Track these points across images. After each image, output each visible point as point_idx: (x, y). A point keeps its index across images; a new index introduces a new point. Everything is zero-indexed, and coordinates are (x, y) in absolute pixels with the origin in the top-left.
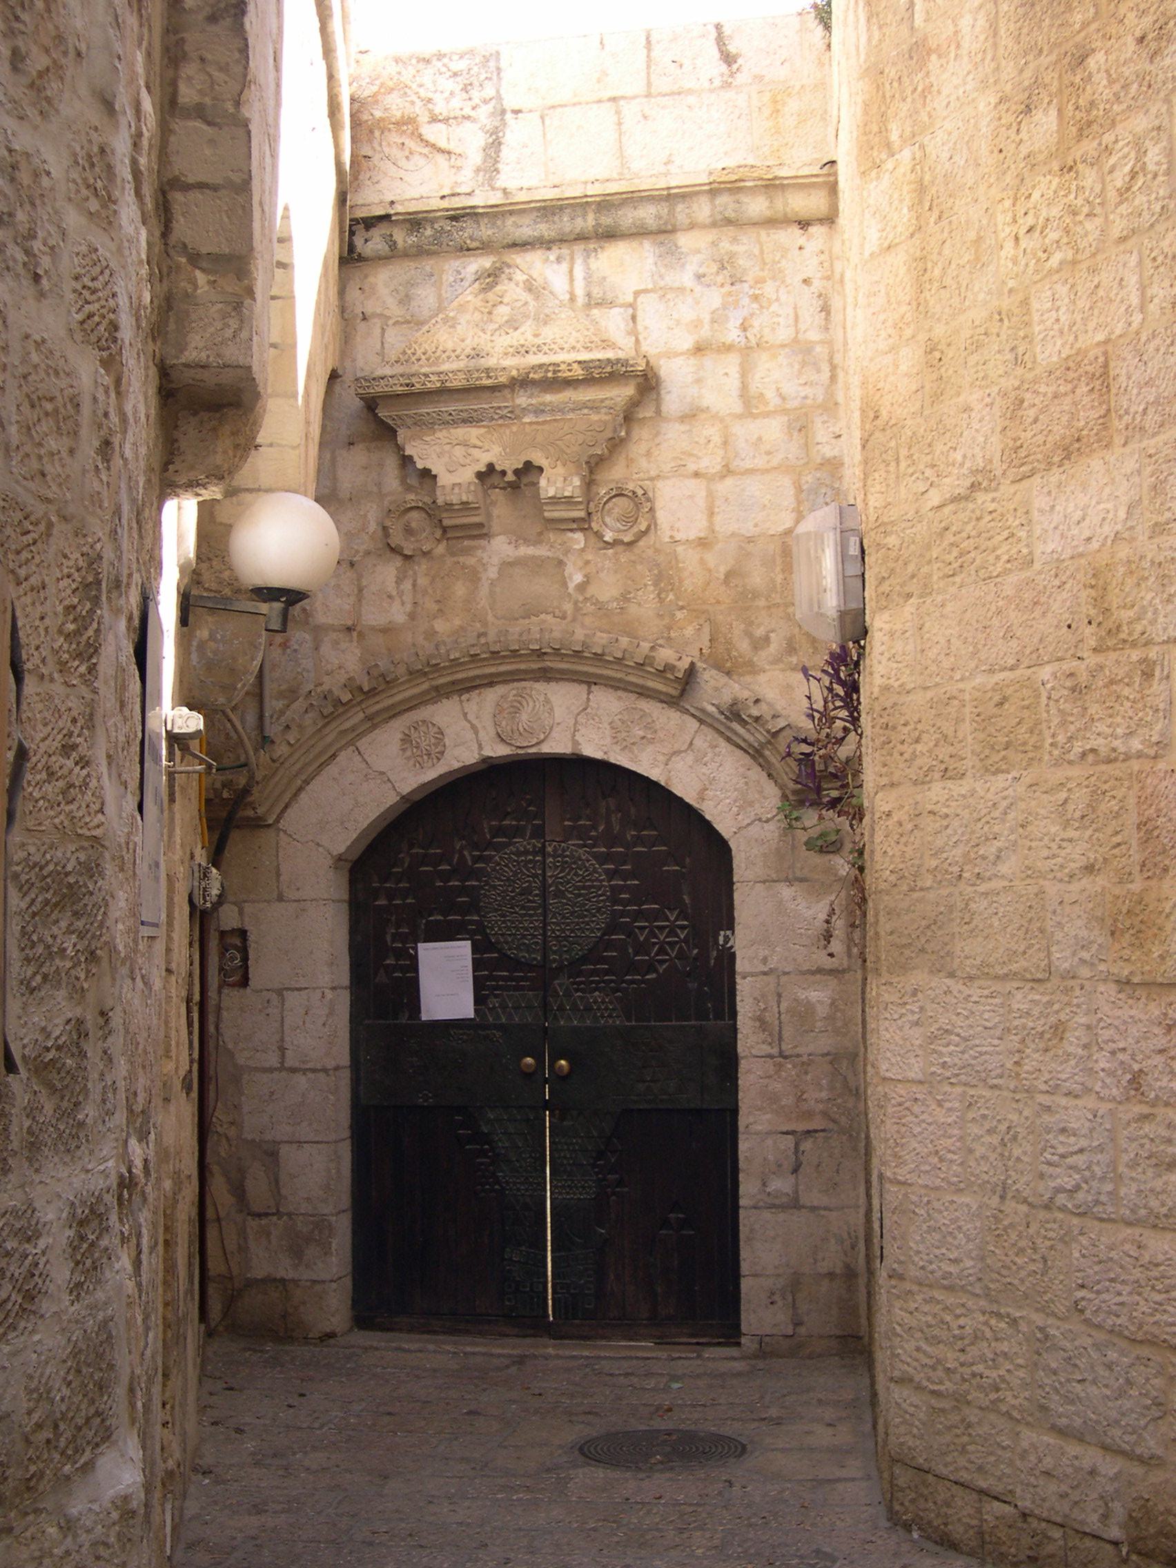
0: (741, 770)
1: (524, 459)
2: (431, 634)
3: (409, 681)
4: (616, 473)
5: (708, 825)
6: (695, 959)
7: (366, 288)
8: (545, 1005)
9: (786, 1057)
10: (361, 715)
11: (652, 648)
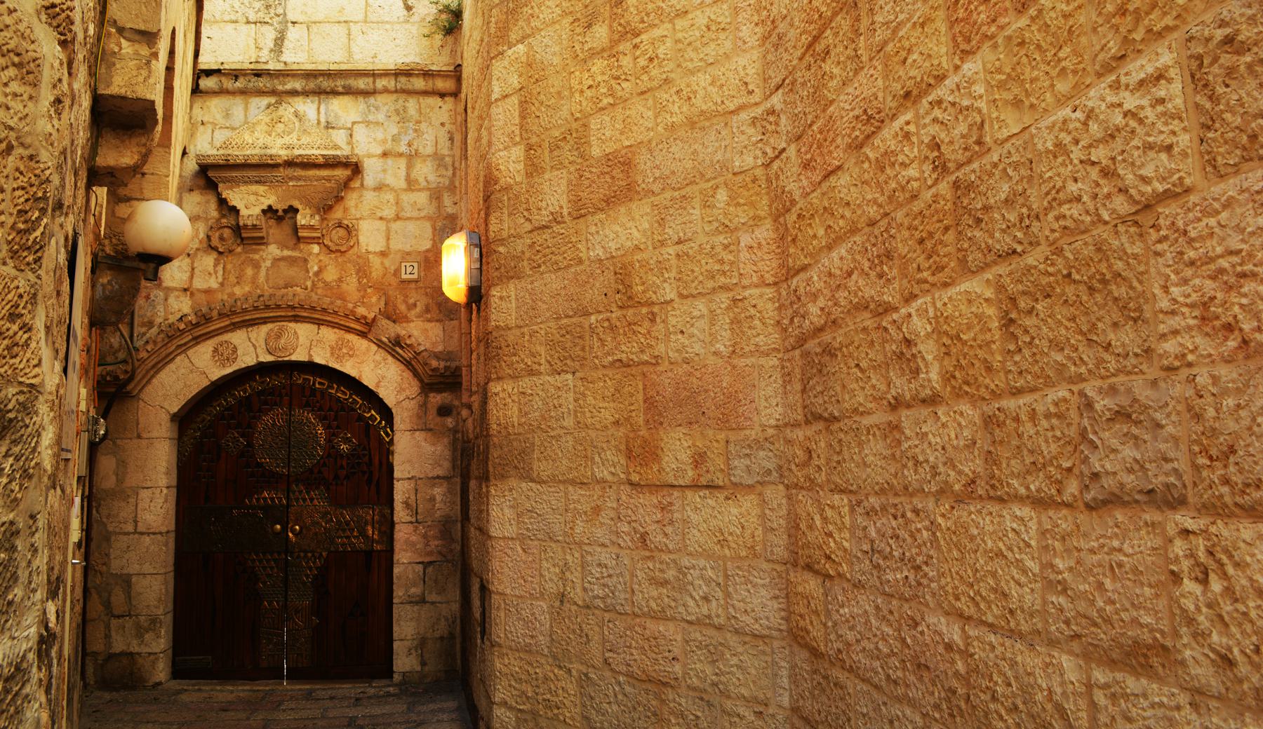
1: (288, 204)
4: (337, 214)
5: (381, 400)
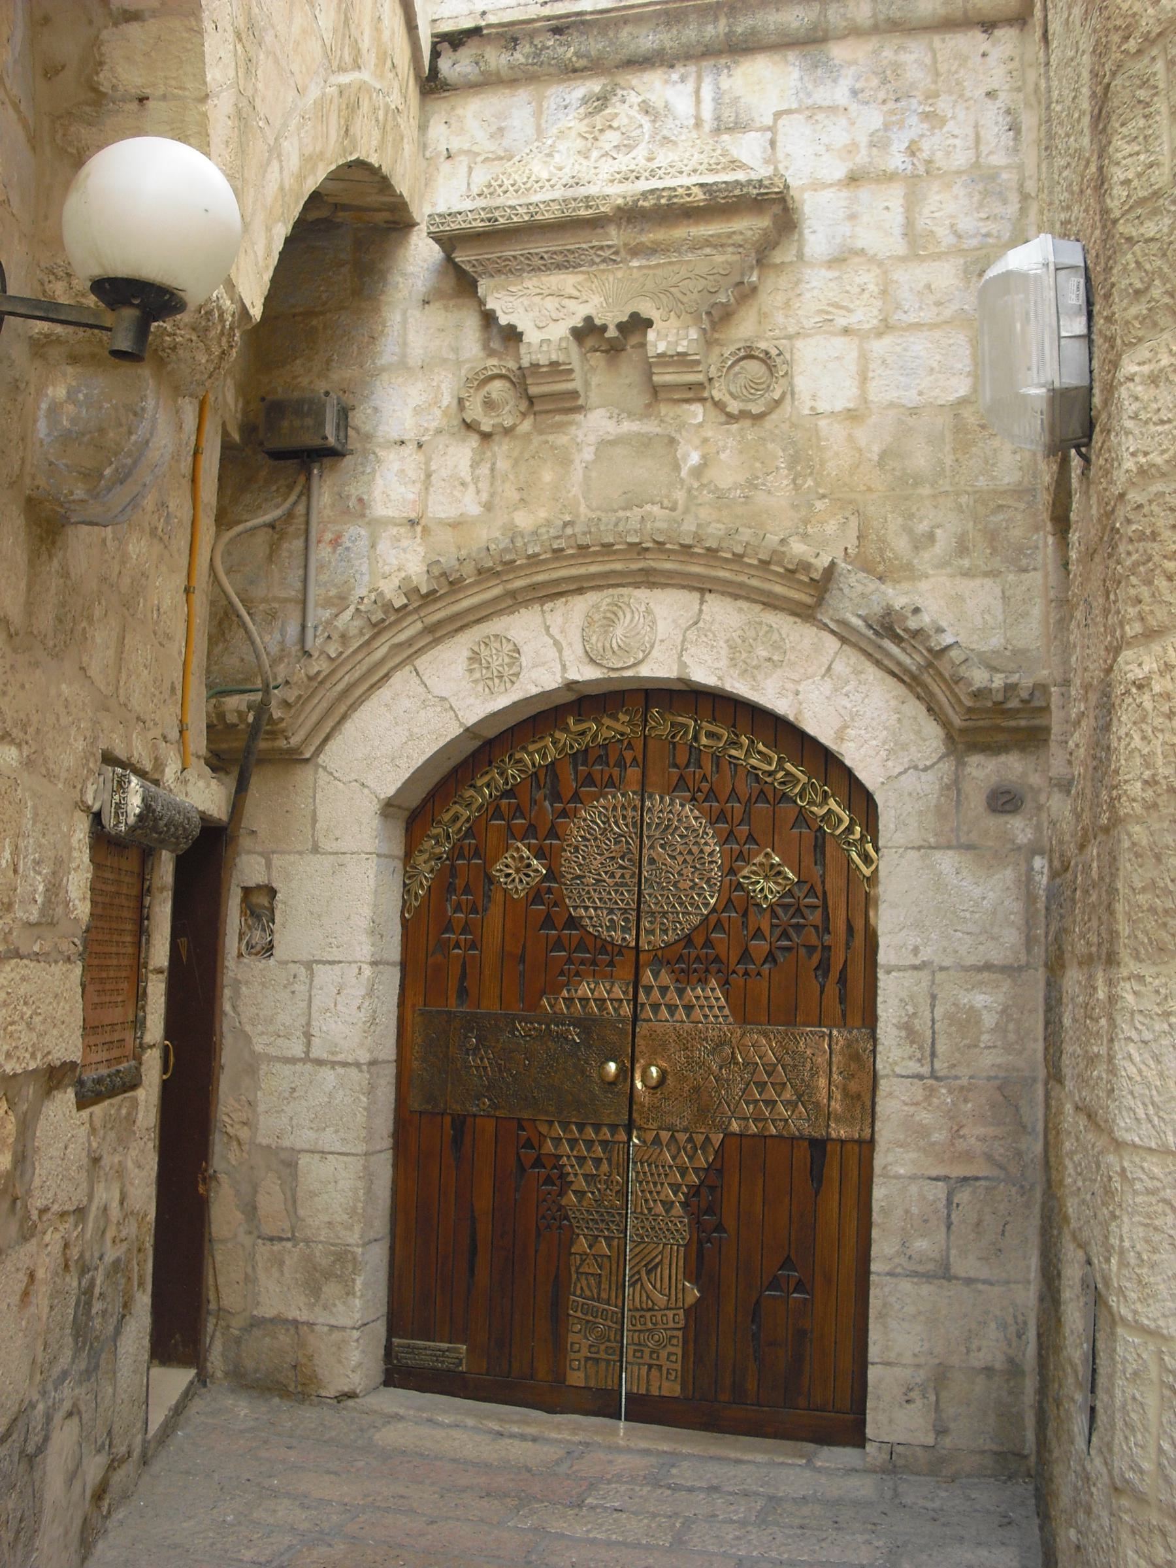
0: (893, 703)
1: (629, 310)
4: (744, 329)
10: (419, 626)
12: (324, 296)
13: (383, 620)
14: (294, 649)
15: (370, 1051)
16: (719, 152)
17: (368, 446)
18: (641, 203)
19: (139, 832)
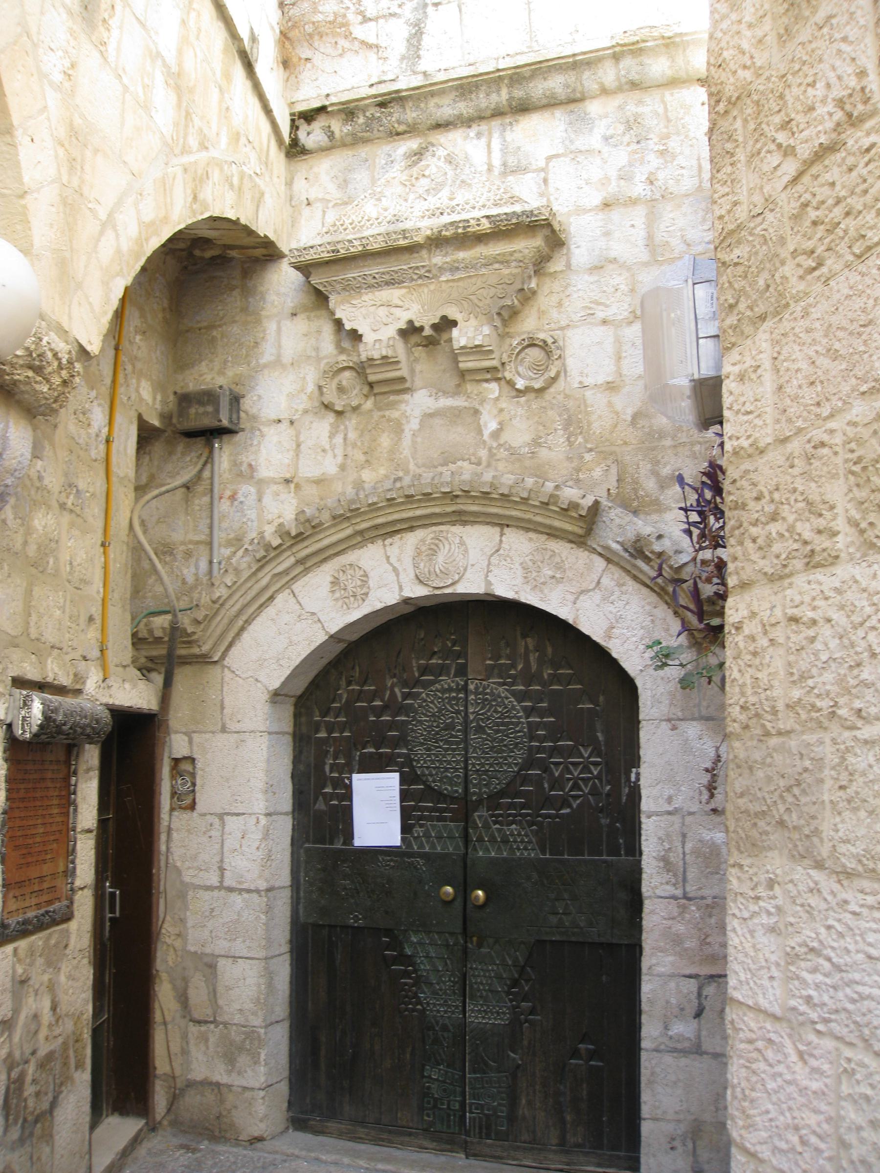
0: (647, 608)
1: (439, 314)
2: (359, 485)
3: (334, 525)
4: (529, 324)
5: (614, 663)
6: (608, 795)
7: (311, 177)
8: (466, 837)
9: (689, 899)
10: (292, 560)
11: (557, 487)
12: (221, 313)
13: (265, 557)
14: (205, 580)
15: (267, 880)
16: (502, 190)
17: (255, 425)
18: (444, 233)
19: (43, 737)
